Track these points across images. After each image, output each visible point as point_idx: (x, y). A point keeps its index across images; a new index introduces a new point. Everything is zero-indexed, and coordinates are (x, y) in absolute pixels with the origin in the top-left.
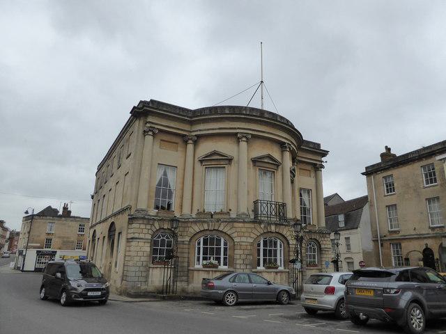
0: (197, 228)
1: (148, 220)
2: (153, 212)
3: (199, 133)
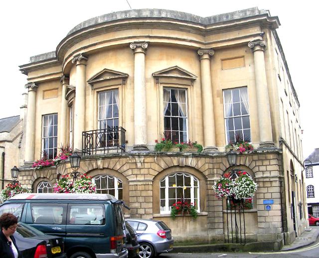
3: (214, 46)
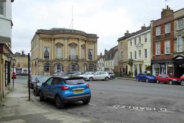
0: (55, 63)
1: (43, 61)
2: (44, 59)
3: (54, 37)
